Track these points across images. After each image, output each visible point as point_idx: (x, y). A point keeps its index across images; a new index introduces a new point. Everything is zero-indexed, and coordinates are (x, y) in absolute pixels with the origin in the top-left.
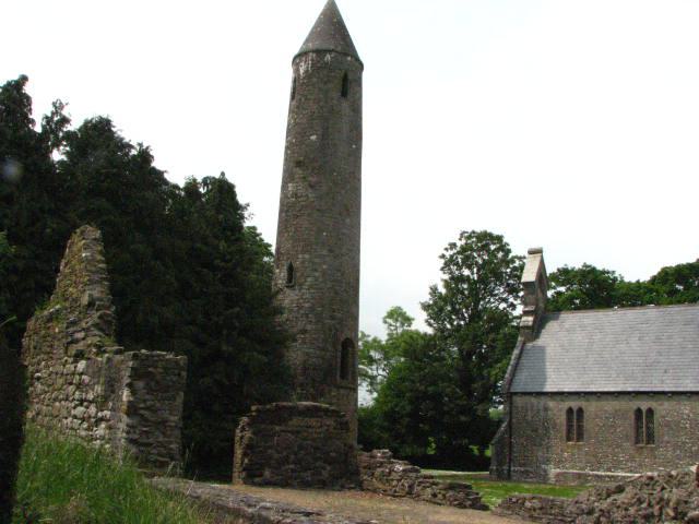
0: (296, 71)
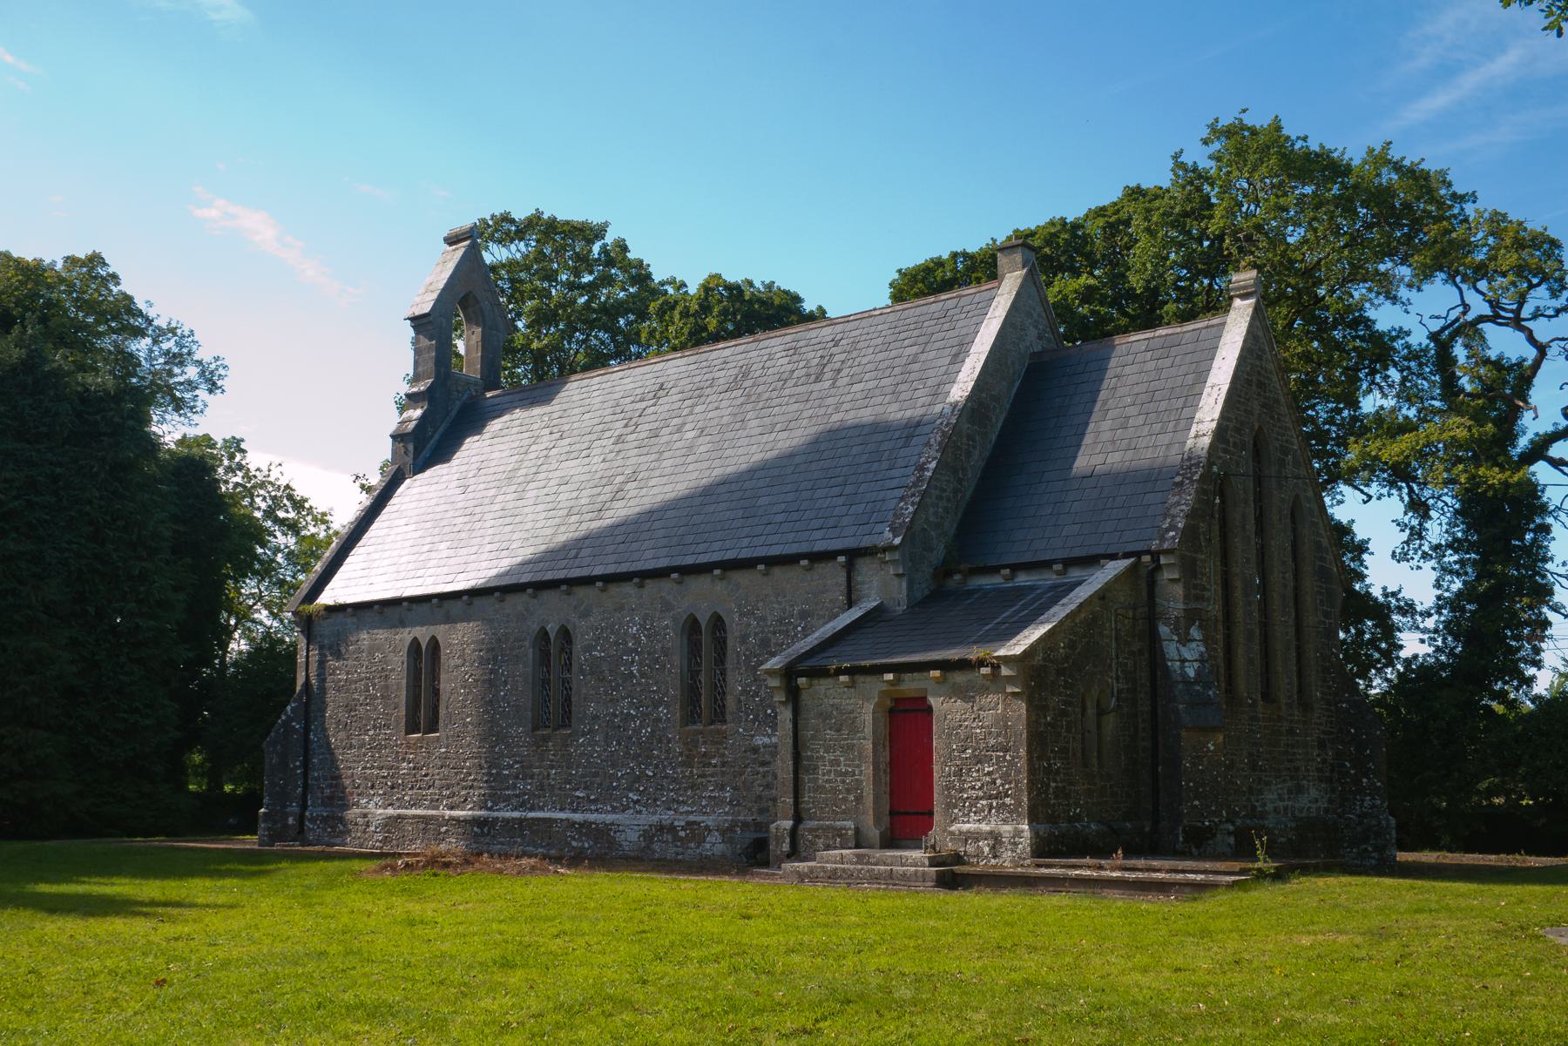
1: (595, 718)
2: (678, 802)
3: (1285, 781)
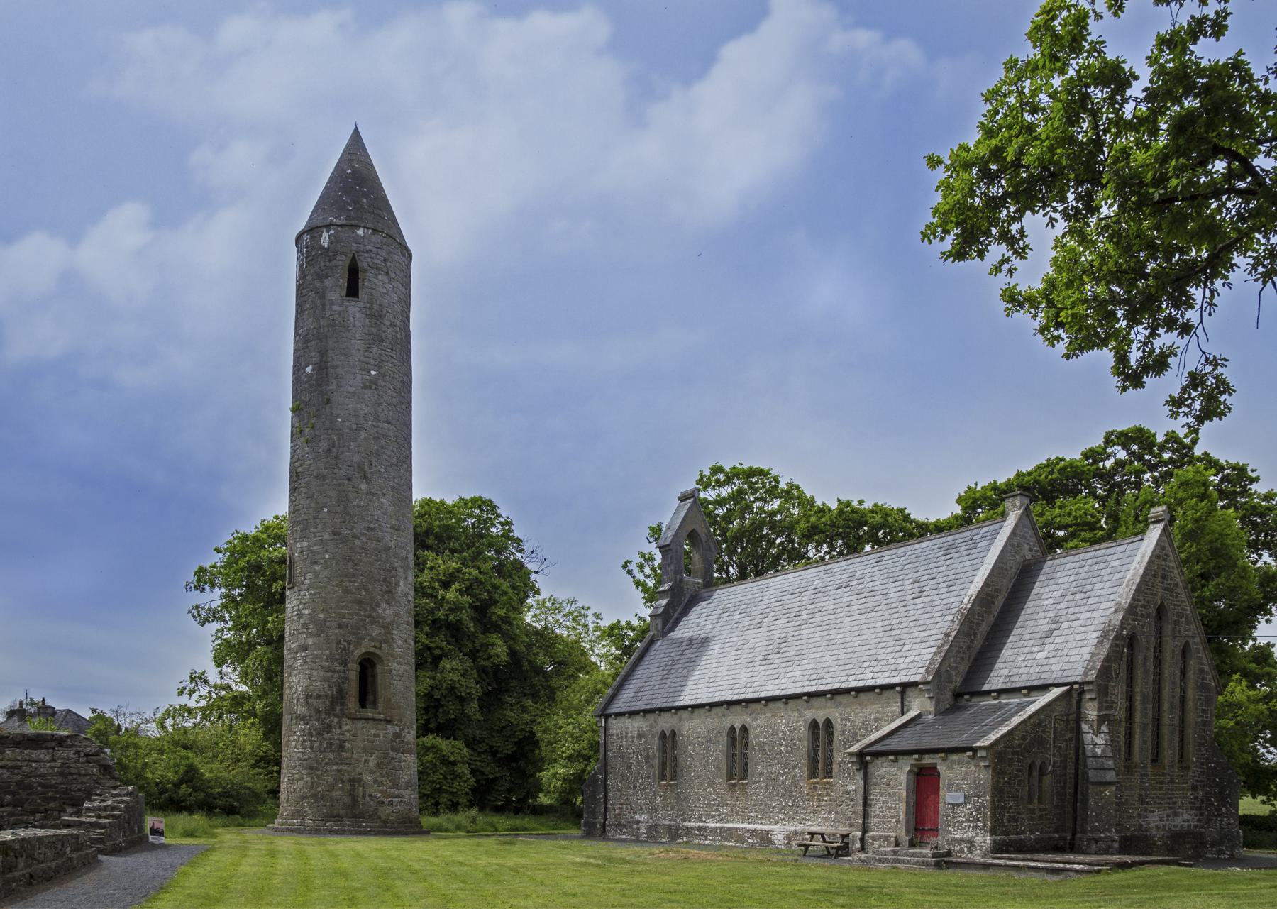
1: (761, 774)
2: (806, 820)
3: (1164, 810)
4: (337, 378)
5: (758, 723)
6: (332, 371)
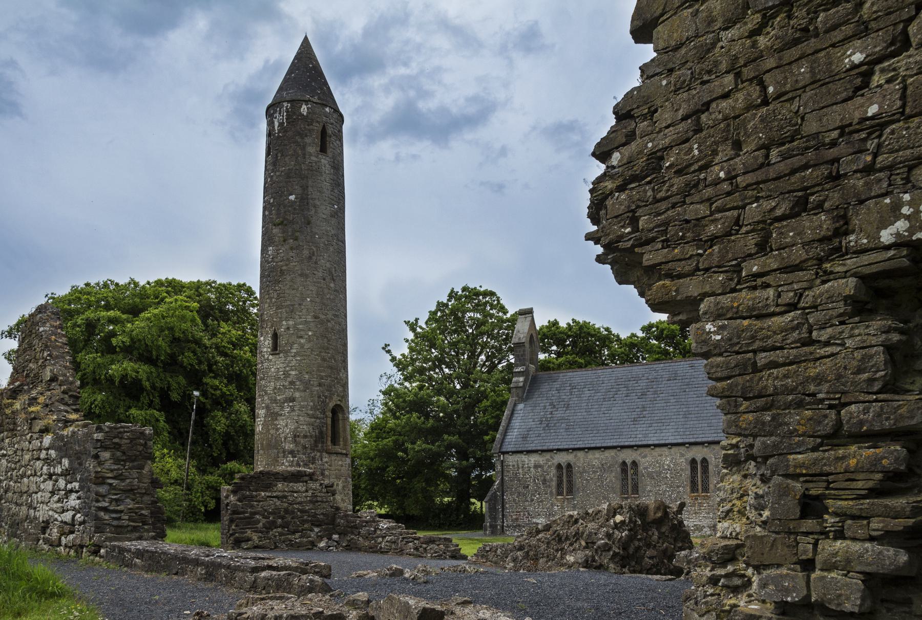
0: (270, 124)
1: (650, 491)
4: (315, 207)
5: (646, 460)
6: (311, 201)
